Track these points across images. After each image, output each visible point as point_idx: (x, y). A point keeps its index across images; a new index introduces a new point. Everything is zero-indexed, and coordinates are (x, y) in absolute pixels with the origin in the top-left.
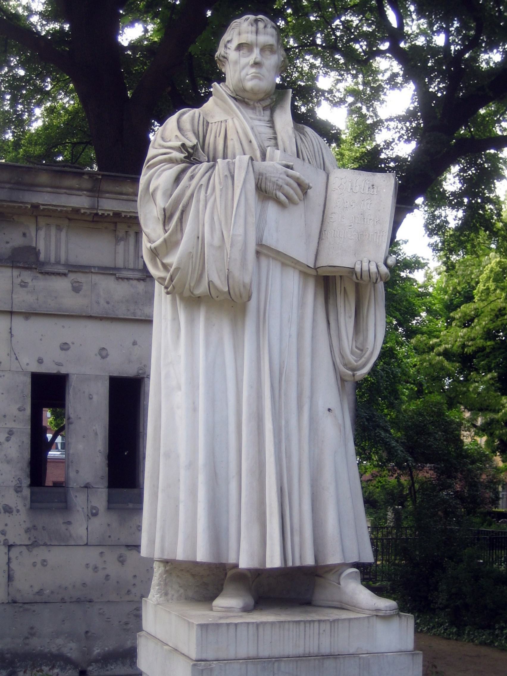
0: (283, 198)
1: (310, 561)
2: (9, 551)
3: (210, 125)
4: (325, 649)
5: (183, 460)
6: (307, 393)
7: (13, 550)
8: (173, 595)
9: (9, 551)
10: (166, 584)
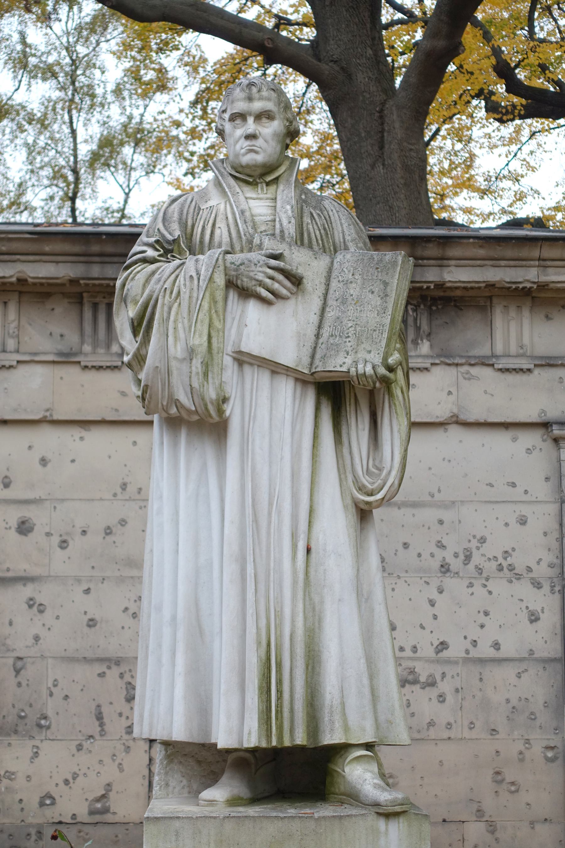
0: (264, 293)
1: (300, 739)
2: (150, 747)
3: (201, 211)
8: (174, 788)
9: (150, 747)
10: (166, 773)
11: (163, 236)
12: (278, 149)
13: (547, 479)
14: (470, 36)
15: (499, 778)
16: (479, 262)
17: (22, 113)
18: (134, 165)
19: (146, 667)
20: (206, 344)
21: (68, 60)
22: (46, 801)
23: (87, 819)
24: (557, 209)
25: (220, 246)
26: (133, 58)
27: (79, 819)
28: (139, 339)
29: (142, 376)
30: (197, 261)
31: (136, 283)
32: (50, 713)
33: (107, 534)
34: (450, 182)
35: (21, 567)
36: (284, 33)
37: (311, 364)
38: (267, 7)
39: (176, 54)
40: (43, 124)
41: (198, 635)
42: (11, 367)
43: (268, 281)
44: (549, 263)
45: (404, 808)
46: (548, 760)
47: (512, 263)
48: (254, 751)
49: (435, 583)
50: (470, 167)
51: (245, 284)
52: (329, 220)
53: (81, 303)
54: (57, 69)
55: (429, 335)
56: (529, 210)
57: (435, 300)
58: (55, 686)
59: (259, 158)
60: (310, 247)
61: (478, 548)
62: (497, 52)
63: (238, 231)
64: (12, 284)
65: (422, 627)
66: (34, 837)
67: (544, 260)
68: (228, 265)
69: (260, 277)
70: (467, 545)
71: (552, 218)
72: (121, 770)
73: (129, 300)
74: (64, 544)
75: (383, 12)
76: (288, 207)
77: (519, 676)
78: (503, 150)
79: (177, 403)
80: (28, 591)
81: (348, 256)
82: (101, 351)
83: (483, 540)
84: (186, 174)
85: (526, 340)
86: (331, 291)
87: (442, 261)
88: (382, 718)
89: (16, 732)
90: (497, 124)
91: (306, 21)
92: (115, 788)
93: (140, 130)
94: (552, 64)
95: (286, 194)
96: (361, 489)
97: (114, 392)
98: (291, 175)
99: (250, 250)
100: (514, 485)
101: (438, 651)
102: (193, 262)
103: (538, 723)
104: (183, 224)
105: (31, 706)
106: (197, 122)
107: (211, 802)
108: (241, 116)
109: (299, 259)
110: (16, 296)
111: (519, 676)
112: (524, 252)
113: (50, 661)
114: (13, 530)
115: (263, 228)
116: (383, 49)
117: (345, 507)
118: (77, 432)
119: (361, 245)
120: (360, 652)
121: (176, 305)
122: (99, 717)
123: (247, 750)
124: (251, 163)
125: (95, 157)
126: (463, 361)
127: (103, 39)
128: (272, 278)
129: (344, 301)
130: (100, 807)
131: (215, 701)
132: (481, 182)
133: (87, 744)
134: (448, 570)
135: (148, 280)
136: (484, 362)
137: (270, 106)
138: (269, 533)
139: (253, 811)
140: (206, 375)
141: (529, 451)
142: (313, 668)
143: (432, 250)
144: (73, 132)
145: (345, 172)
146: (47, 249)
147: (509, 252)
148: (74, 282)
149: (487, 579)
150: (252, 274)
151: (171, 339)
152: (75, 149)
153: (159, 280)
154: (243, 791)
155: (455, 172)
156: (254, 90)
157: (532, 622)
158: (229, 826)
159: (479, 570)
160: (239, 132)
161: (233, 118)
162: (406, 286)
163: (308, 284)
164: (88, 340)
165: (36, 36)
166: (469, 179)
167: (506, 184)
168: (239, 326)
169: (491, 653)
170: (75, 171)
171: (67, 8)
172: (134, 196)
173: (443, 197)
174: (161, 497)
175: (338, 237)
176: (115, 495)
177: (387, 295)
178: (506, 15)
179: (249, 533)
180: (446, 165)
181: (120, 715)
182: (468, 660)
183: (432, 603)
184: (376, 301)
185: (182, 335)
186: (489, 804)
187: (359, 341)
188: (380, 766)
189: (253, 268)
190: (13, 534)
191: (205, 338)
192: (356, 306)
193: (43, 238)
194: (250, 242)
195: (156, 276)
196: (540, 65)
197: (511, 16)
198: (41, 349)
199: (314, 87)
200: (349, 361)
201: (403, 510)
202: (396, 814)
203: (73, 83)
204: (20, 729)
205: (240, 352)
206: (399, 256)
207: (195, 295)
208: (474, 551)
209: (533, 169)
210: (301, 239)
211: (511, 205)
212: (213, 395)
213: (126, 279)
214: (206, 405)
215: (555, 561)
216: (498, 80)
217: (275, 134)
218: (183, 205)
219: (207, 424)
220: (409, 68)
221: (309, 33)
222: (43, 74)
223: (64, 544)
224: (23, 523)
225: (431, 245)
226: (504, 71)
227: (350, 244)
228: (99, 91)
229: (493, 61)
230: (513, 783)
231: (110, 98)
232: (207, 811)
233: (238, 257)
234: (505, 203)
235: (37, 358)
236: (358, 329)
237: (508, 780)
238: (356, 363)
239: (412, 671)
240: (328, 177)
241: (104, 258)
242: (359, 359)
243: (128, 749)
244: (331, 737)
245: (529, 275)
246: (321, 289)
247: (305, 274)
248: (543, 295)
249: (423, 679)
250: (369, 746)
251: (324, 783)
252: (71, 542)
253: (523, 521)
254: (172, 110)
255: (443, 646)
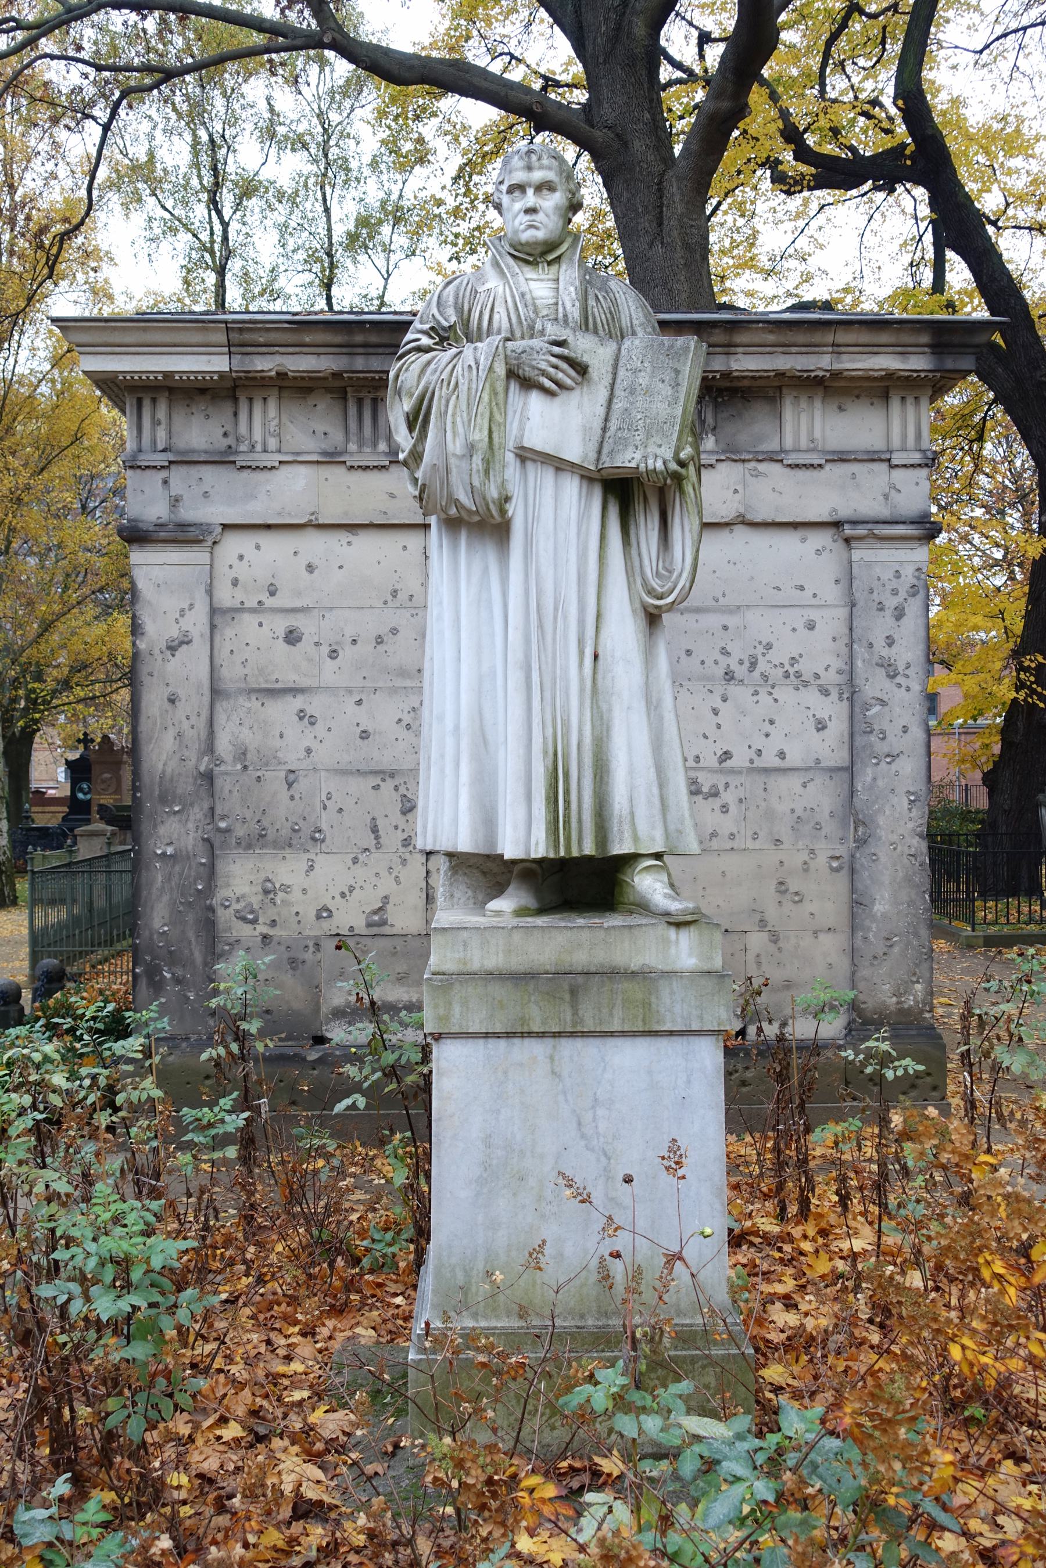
0: (548, 383)
1: (589, 848)
7: (432, 858)
10: (451, 885)
11: (438, 322)
12: (561, 223)
13: (837, 581)
14: (757, 96)
15: (783, 888)
16: (768, 349)
17: (271, 190)
18: (393, 248)
19: (428, 778)
20: (487, 439)
21: (320, 129)
22: (324, 913)
24: (846, 290)
25: (499, 332)
26: (389, 127)
27: (356, 932)
28: (415, 434)
29: (419, 474)
30: (475, 349)
31: (410, 373)
32: (324, 827)
33: (378, 643)
34: (731, 262)
35: (290, 678)
36: (553, 96)
37: (598, 460)
38: (534, 66)
39: (435, 122)
40: (293, 200)
41: (483, 744)
42: (273, 468)
43: (551, 370)
44: (843, 349)
45: (695, 917)
46: (832, 869)
47: (803, 349)
49: (719, 690)
50: (753, 245)
51: (527, 374)
52: (615, 302)
53: (345, 399)
54: (307, 138)
55: (714, 429)
56: (814, 293)
57: (720, 391)
58: (329, 799)
59: (540, 235)
60: (596, 332)
61: (764, 655)
62: (784, 114)
63: (519, 316)
64: (271, 378)
65: (705, 737)
66: (312, 949)
67: (839, 346)
68: (509, 353)
69: (543, 366)
70: (752, 652)
71: (840, 301)
72: (398, 883)
73: (403, 394)
74: (333, 654)
75: (662, 70)
76: (572, 289)
78: (789, 226)
79: (457, 503)
80: (298, 702)
81: (637, 342)
83: (769, 646)
84: (450, 260)
85: (817, 434)
86: (618, 381)
87: (728, 348)
88: (672, 827)
89: (290, 845)
90: (783, 196)
91: (576, 82)
92: (392, 900)
93: (398, 208)
94: (844, 128)
95: (569, 274)
96: (651, 592)
97: (390, 493)
98: (574, 254)
99: (532, 337)
100: (802, 588)
102: (471, 350)
103: (823, 833)
104: (459, 309)
105: (305, 819)
106: (460, 198)
107: (498, 913)
108: (518, 188)
109: (583, 346)
110: (275, 392)
112: (817, 338)
113: (323, 773)
114: (281, 640)
115: (545, 312)
116: (662, 112)
117: (634, 611)
118: (344, 536)
119: (649, 330)
120: (650, 762)
121: (454, 397)
122: (375, 830)
123: (535, 861)
124: (531, 240)
125: (353, 237)
126: (751, 457)
127: (357, 104)
128: (556, 367)
129: (632, 392)
130: (378, 918)
131: (501, 811)
132: (764, 262)
133: (362, 858)
134: (733, 678)
135: (423, 371)
136: (773, 458)
137: (551, 175)
138: (554, 639)
139: (541, 921)
140: (487, 472)
142: (601, 777)
143: (719, 337)
144: (327, 210)
145: (620, 251)
147: (801, 338)
148: (337, 375)
149: (773, 687)
150: (534, 363)
151: (449, 434)
152: (329, 230)
153: (435, 371)
154: (530, 902)
155: (735, 252)
156: (534, 158)
157: (818, 730)
158: (517, 937)
159: (765, 677)
160: (518, 206)
161: (510, 190)
162: (698, 375)
163: (594, 373)
164: (354, 438)
165: (285, 101)
166: (752, 259)
167: (792, 263)
168: (521, 421)
169: (777, 762)
170: (330, 255)
171: (318, 69)
172: (397, 281)
173: (723, 278)
174: (441, 603)
175: (625, 321)
176: (385, 602)
177: (678, 385)
178: (795, 72)
179: (534, 639)
180: (727, 243)
181: (396, 828)
184: (667, 390)
185: (460, 429)
186: (772, 914)
187: (649, 435)
188: (669, 875)
189: (535, 356)
191: (486, 433)
192: (645, 397)
193: (301, 329)
194: (532, 328)
195: (432, 366)
196: (831, 129)
197: (802, 74)
198: (304, 448)
199: (586, 156)
200: (638, 456)
201: (686, 616)
202: (687, 924)
203: (326, 156)
204: (294, 842)
205: (523, 448)
206: (690, 341)
207: (474, 386)
208: (760, 657)
209: (822, 247)
210: (586, 324)
211: (796, 288)
212: (495, 495)
213: (400, 369)
214: (487, 505)
215: (844, 667)
216: (785, 146)
217: (557, 208)
218: (458, 288)
219: (487, 525)
220: (691, 135)
221: (580, 96)
222: (293, 144)
223: (333, 654)
224: (291, 632)
225: (717, 331)
226: (792, 135)
227: (638, 329)
228: (354, 165)
229: (780, 124)
230: (797, 894)
231: (367, 172)
232: (494, 921)
233: (519, 345)
234: (790, 285)
235: (300, 459)
236: (648, 421)
237: (792, 890)
238: (645, 458)
240: (600, 258)
241: (368, 349)
242: (649, 455)
243: (404, 862)
244: (620, 847)
245: (822, 363)
246: (607, 380)
247: (590, 362)
248: (836, 384)
250: (658, 856)
251: (613, 895)
252: (341, 653)
253: (811, 626)
254: (434, 188)
255: (727, 755)
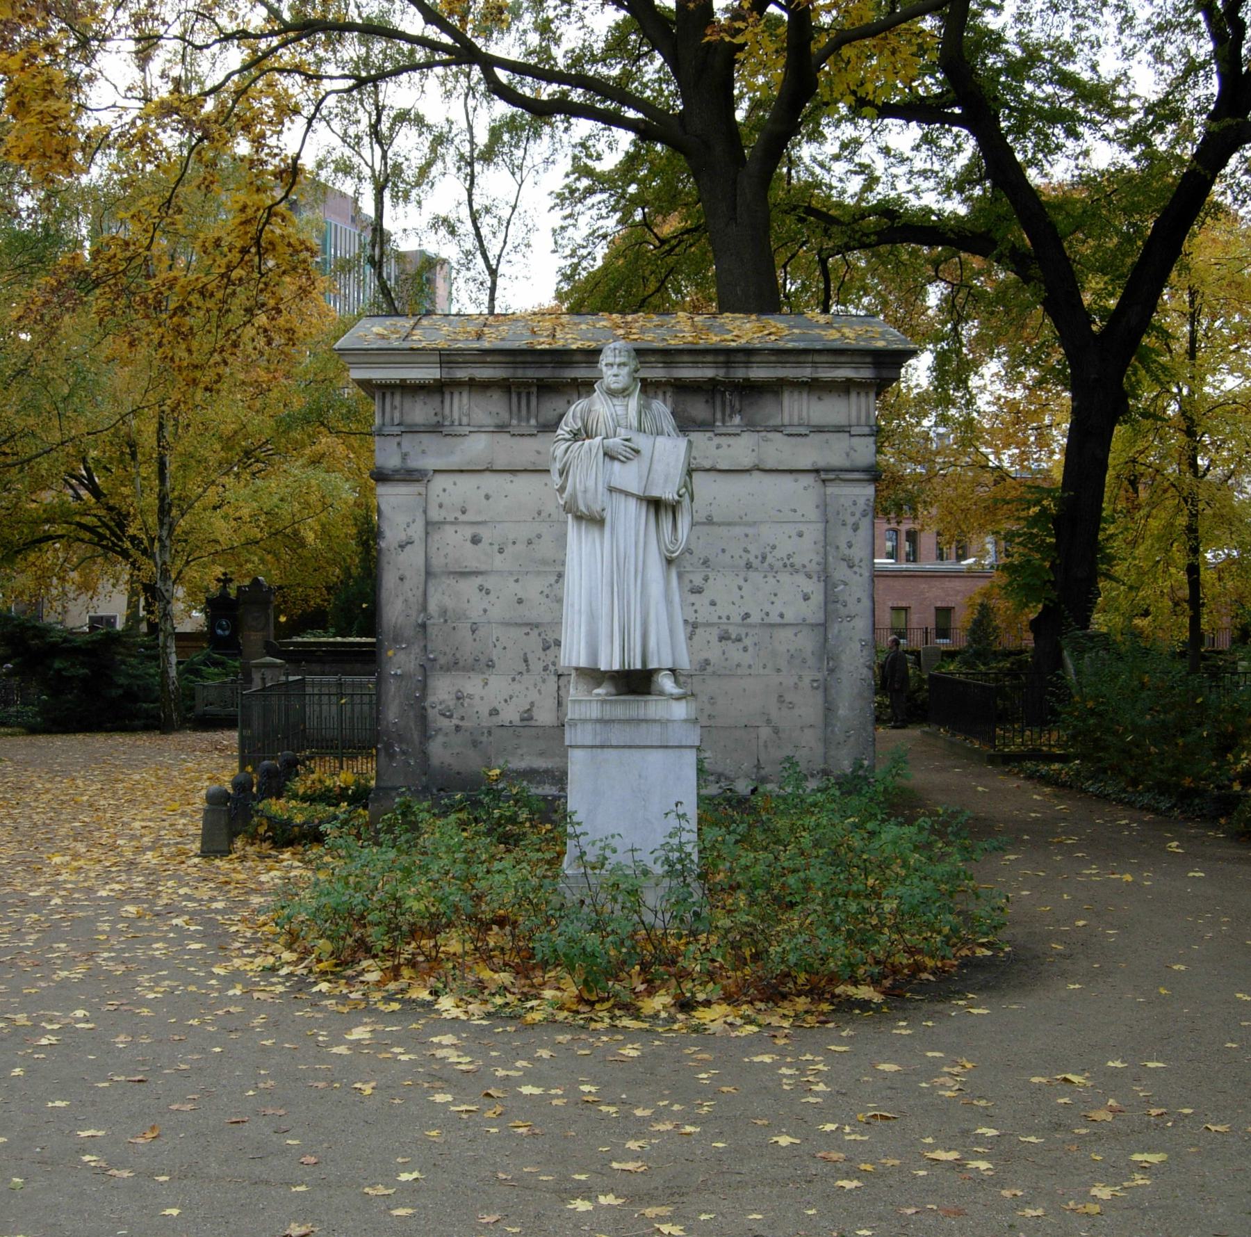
1: (639, 666)
4: (642, 716)
5: (576, 607)
6: (640, 568)
13: (817, 507)
22: (494, 712)
23: (519, 723)
32: (495, 658)
35: (473, 565)
48: (617, 672)
49: (742, 574)
53: (510, 392)
74: (501, 551)
77: (796, 635)
80: (479, 580)
82: (523, 424)
83: (774, 547)
85: (804, 414)
87: (747, 364)
100: (795, 511)
101: (743, 619)
104: (583, 420)
107: (598, 695)
111: (796, 635)
112: (802, 359)
118: (508, 477)
122: (526, 661)
133: (518, 677)
136: (776, 429)
141: (805, 488)
146: (489, 359)
147: (792, 359)
154: (612, 690)
159: (771, 567)
169: (779, 620)
182: (764, 625)
183: (740, 588)
190: (469, 544)
198: (484, 422)
219: (595, 521)
223: (501, 551)
239: (727, 632)
243: (544, 681)
244: (653, 665)
245: (806, 373)
249: (733, 637)
253: (800, 535)
255: (747, 615)
